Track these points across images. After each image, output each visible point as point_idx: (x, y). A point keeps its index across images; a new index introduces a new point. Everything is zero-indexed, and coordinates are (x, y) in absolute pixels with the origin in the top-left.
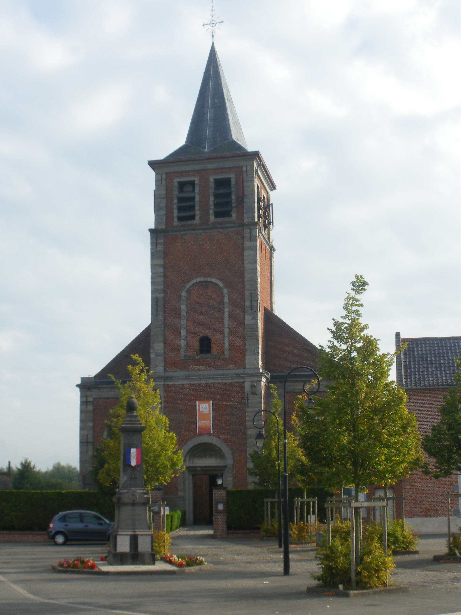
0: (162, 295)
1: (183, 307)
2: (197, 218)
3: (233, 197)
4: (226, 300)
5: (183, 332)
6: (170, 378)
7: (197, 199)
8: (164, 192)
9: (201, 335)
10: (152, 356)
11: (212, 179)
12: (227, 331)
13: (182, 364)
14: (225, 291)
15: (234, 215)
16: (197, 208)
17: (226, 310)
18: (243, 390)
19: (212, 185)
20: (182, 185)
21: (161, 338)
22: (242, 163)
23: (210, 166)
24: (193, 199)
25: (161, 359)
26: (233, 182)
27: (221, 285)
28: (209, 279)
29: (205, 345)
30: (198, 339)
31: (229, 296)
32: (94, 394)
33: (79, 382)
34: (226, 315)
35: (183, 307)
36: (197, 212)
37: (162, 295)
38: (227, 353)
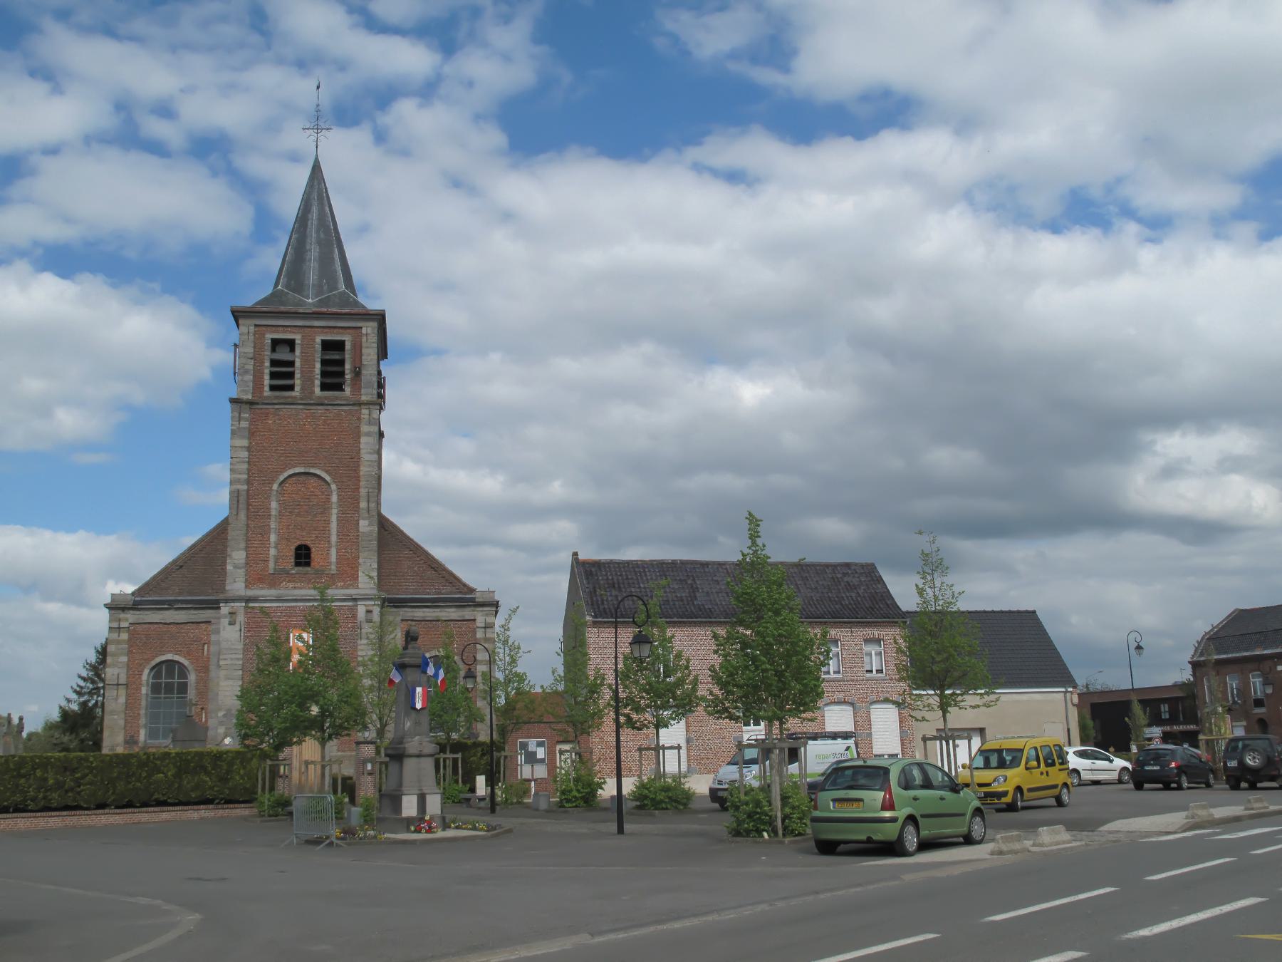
0: (245, 487)
1: (274, 505)
2: (297, 388)
3: (348, 366)
4: (334, 498)
5: (273, 538)
6: (255, 600)
7: (298, 363)
8: (252, 350)
9: (299, 543)
10: (229, 567)
11: (318, 340)
12: (334, 538)
13: (273, 580)
14: (334, 487)
15: (348, 390)
16: (297, 376)
17: (334, 511)
18: (355, 617)
19: (319, 347)
20: (327, 346)
21: (243, 545)
22: (359, 324)
23: (316, 323)
24: (292, 364)
25: (242, 572)
26: (348, 346)
27: (328, 478)
28: (312, 471)
29: (303, 556)
30: (293, 548)
31: (339, 495)
32: (131, 617)
33: (109, 600)
34: (334, 518)
35: (274, 505)
36: (297, 382)
37: (245, 487)
38: (333, 567)
